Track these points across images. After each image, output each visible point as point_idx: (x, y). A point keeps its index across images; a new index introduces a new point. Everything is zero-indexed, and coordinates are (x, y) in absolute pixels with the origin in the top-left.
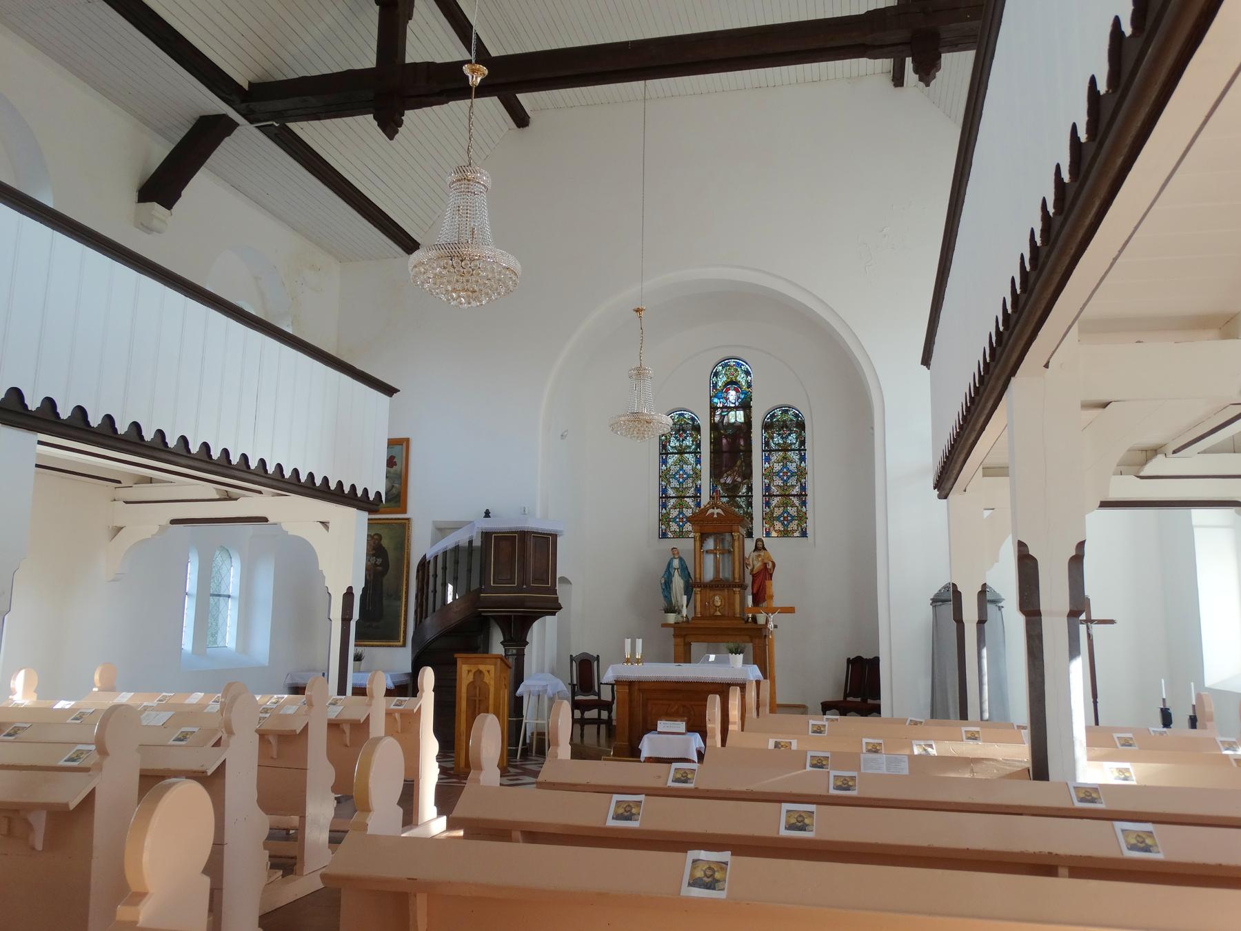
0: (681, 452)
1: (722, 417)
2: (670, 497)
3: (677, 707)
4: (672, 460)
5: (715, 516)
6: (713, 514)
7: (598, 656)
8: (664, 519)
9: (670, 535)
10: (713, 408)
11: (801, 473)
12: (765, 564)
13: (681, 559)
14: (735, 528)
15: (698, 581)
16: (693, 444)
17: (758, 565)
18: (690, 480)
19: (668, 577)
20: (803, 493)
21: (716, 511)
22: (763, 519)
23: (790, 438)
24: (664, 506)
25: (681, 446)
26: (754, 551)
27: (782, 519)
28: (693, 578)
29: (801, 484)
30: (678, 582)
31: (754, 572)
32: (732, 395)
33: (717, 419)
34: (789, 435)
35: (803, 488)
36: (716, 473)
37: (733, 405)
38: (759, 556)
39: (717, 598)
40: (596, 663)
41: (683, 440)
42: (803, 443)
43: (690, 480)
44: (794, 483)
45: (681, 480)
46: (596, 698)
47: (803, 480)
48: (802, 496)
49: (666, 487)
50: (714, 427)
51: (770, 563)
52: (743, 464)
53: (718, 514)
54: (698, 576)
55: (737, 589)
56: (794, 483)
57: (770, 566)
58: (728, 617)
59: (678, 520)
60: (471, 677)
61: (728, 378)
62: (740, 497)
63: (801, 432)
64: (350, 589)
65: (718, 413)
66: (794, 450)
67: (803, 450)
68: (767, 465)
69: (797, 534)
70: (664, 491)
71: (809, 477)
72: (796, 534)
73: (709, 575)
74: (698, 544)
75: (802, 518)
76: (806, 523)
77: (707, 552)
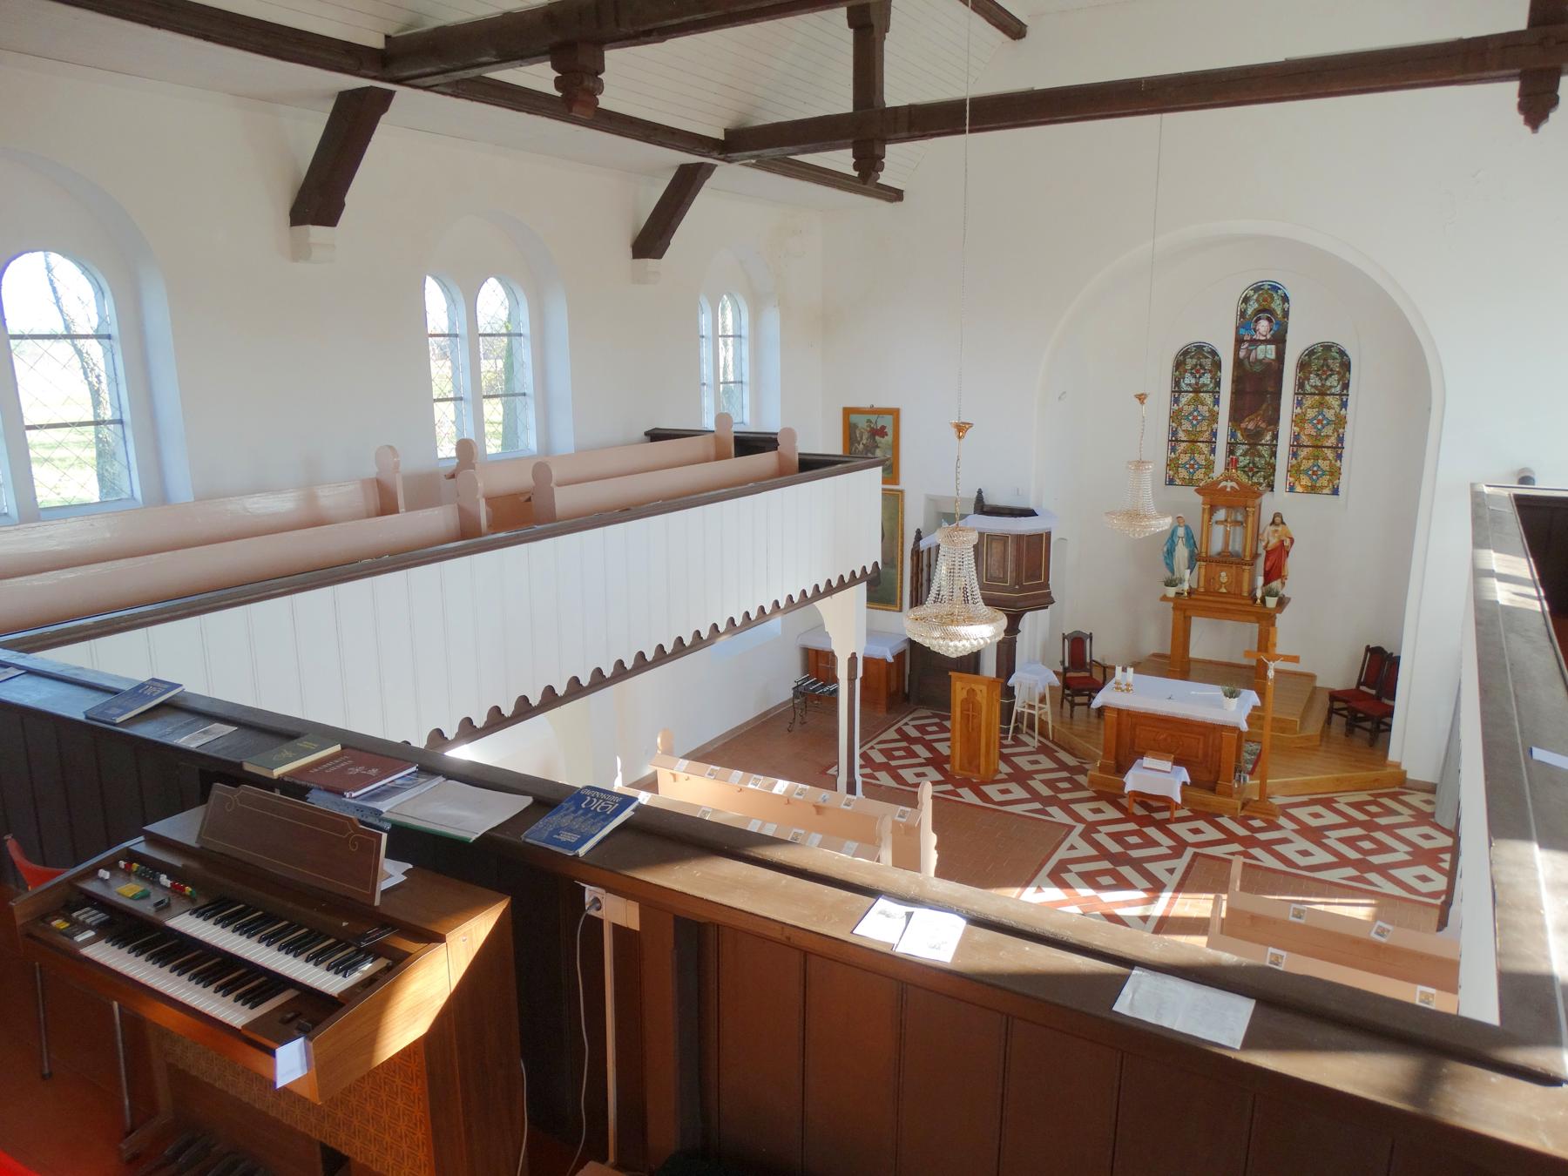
0: (1197, 390)
1: (1249, 352)
2: (1181, 441)
3: (1165, 736)
4: (1184, 399)
5: (1228, 489)
6: (1226, 487)
7: (1091, 634)
8: (1173, 464)
9: (1178, 482)
10: (1239, 341)
11: (1341, 422)
12: (1282, 542)
13: (1187, 528)
14: (1250, 503)
15: (1204, 555)
16: (1211, 382)
17: (1274, 541)
18: (1205, 423)
19: (1171, 545)
20: (1340, 445)
21: (1230, 484)
22: (1288, 471)
23: (1330, 379)
24: (1176, 401)
25: (1199, 359)
26: (1271, 524)
27: (1310, 472)
28: (1198, 546)
29: (1338, 435)
30: (1182, 552)
31: (1269, 549)
32: (1263, 325)
33: (1242, 354)
34: (1331, 375)
35: (1341, 439)
36: (1236, 416)
37: (1264, 338)
38: (1276, 531)
39: (1223, 574)
40: (1088, 640)
41: (1200, 377)
42: (1346, 386)
43: (1205, 423)
44: (1330, 433)
45: (1195, 422)
46: (1087, 674)
47: (1341, 431)
48: (1338, 449)
49: (1176, 429)
50: (1238, 363)
51: (1288, 540)
52: (1270, 408)
53: (1232, 487)
54: (1204, 550)
55: (1247, 567)
56: (1330, 433)
57: (1287, 543)
58: (1235, 594)
59: (1188, 466)
60: (964, 694)
61: (1260, 305)
62: (1263, 445)
63: (1345, 374)
64: (854, 654)
65: (1244, 347)
66: (1333, 394)
67: (1344, 395)
68: (1299, 410)
69: (1326, 491)
70: (1174, 433)
71: (1348, 427)
72: (1325, 491)
73: (1217, 546)
74: (1206, 516)
75: (1335, 473)
76: (1344, 428)
77: (1217, 522)
